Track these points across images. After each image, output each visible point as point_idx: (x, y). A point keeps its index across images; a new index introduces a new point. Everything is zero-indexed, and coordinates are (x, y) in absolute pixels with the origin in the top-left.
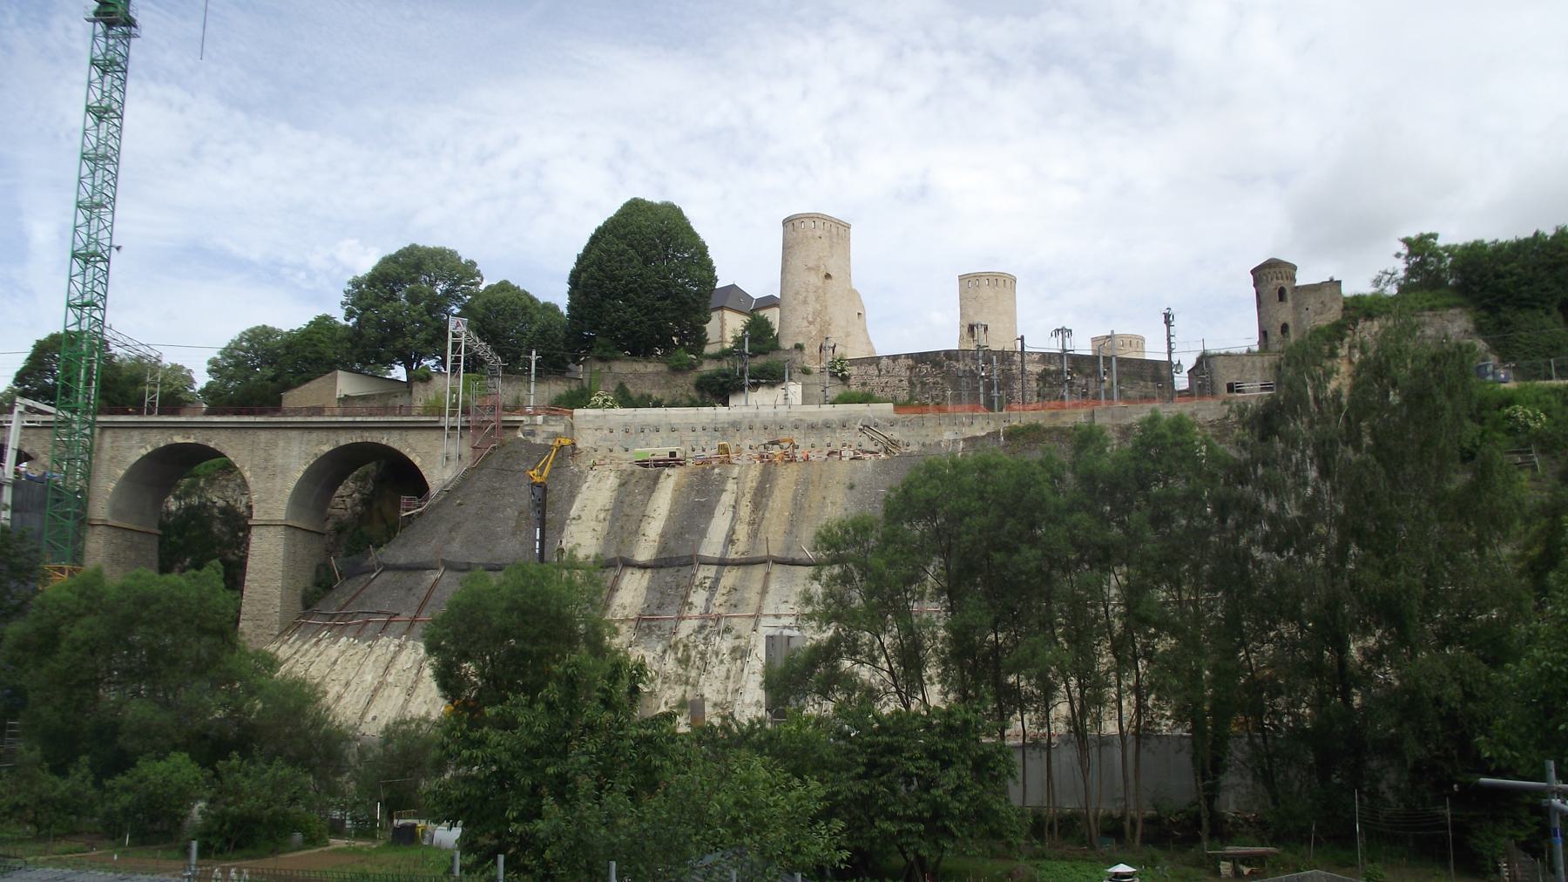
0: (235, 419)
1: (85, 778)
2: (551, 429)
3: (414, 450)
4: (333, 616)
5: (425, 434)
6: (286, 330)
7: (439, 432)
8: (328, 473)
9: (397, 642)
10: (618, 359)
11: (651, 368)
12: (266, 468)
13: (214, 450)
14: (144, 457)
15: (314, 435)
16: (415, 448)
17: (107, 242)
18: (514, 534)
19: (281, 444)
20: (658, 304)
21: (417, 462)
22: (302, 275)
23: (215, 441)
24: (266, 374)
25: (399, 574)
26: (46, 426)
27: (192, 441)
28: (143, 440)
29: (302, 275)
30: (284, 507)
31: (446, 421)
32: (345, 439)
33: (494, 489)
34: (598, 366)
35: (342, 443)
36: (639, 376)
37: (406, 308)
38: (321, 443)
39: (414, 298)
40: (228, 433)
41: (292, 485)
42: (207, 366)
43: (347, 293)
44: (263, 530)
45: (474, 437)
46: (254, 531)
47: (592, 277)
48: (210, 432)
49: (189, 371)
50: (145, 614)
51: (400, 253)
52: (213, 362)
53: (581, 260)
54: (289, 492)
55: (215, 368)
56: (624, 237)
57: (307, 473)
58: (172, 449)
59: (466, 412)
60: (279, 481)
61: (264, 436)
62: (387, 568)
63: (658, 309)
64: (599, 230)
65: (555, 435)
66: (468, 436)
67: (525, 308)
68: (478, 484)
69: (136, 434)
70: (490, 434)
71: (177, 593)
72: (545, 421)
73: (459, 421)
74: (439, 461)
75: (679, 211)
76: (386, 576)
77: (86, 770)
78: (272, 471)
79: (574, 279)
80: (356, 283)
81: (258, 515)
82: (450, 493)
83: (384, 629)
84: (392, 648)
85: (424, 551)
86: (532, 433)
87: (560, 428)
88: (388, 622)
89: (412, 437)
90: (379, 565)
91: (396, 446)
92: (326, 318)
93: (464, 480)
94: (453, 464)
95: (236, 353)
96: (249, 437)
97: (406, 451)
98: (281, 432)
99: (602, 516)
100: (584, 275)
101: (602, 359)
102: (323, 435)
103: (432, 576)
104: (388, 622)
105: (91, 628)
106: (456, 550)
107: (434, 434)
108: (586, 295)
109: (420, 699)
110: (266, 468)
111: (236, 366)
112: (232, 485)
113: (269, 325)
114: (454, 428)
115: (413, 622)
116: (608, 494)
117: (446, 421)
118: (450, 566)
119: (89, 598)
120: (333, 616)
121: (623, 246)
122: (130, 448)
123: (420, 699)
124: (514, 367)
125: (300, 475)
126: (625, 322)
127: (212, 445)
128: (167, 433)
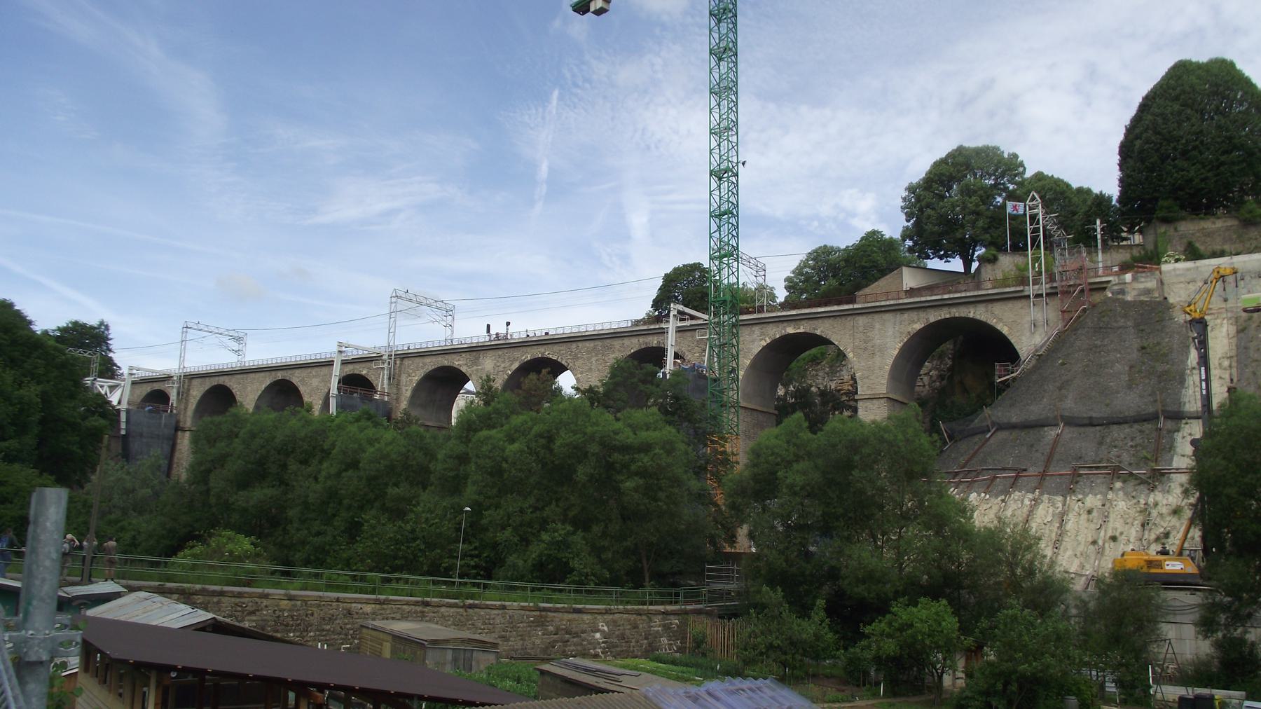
0: (836, 308)
1: (822, 621)
2: (1142, 286)
3: (1000, 320)
4: (956, 474)
5: (1010, 304)
6: (843, 247)
7: (1024, 302)
8: (920, 348)
9: (1030, 496)
10: (1183, 219)
11: (1219, 224)
12: (865, 349)
13: (820, 337)
14: (764, 348)
15: (906, 316)
16: (1002, 319)
17: (735, 160)
18: (1130, 387)
19: (877, 326)
20: (1223, 158)
21: (1005, 331)
22: (816, 223)
23: (821, 329)
24: (842, 276)
25: (1015, 433)
26: (692, 329)
27: (801, 330)
28: (762, 334)
29: (816, 223)
30: (884, 381)
31: (1031, 290)
32: (934, 316)
33: (1096, 347)
34: (1162, 229)
35: (932, 320)
36: (1209, 234)
37: (965, 204)
38: (913, 322)
39: (967, 192)
40: (830, 321)
41: (890, 361)
42: (783, 284)
43: (904, 199)
44: (868, 404)
45: (1062, 301)
46: (860, 404)
47: (1147, 141)
48: (815, 322)
49: (772, 288)
50: (857, 458)
51: (950, 155)
52: (788, 279)
53: (1130, 131)
54: (888, 368)
55: (791, 285)
56: (1177, 98)
57: (902, 350)
58: (786, 339)
59: (1051, 278)
60: (877, 359)
61: (861, 320)
62: (1001, 427)
63: (1223, 164)
64: (1146, 98)
65: (1148, 292)
66: (1056, 302)
67: (1062, 193)
68: (1078, 343)
69: (756, 329)
70: (1078, 297)
71: (886, 436)
72: (1134, 279)
73: (1044, 288)
74: (1028, 329)
75: (1232, 64)
76: (1002, 435)
77: (822, 614)
78: (871, 351)
79: (1127, 151)
80: (911, 189)
81: (862, 391)
82: (1043, 358)
83: (1014, 484)
84: (1027, 502)
85: (1036, 410)
86: (1122, 292)
87: (1151, 284)
88: (1017, 477)
89: (998, 308)
90: (993, 424)
91: (983, 318)
92: (874, 233)
93: (1059, 344)
94: (1041, 330)
95: (805, 270)
96: (849, 322)
97: (993, 322)
98: (876, 316)
99: (1226, 363)
100: (1138, 143)
101: (1166, 221)
102: (914, 315)
103: (1052, 433)
104: (1017, 477)
105: (804, 473)
106: (1070, 405)
107: (1018, 304)
108: (1143, 161)
109: (1069, 553)
110: (865, 349)
111: (807, 280)
112: (821, 374)
113: (829, 244)
114: (1039, 296)
115: (1043, 476)
116: (1226, 341)
117: (1031, 290)
118: (1071, 422)
119: (795, 445)
120: (956, 474)
121: (1176, 107)
122: (753, 341)
123: (1069, 553)
124: (1085, 239)
125: (896, 352)
126: (1191, 180)
127: (818, 332)
128: (781, 326)
